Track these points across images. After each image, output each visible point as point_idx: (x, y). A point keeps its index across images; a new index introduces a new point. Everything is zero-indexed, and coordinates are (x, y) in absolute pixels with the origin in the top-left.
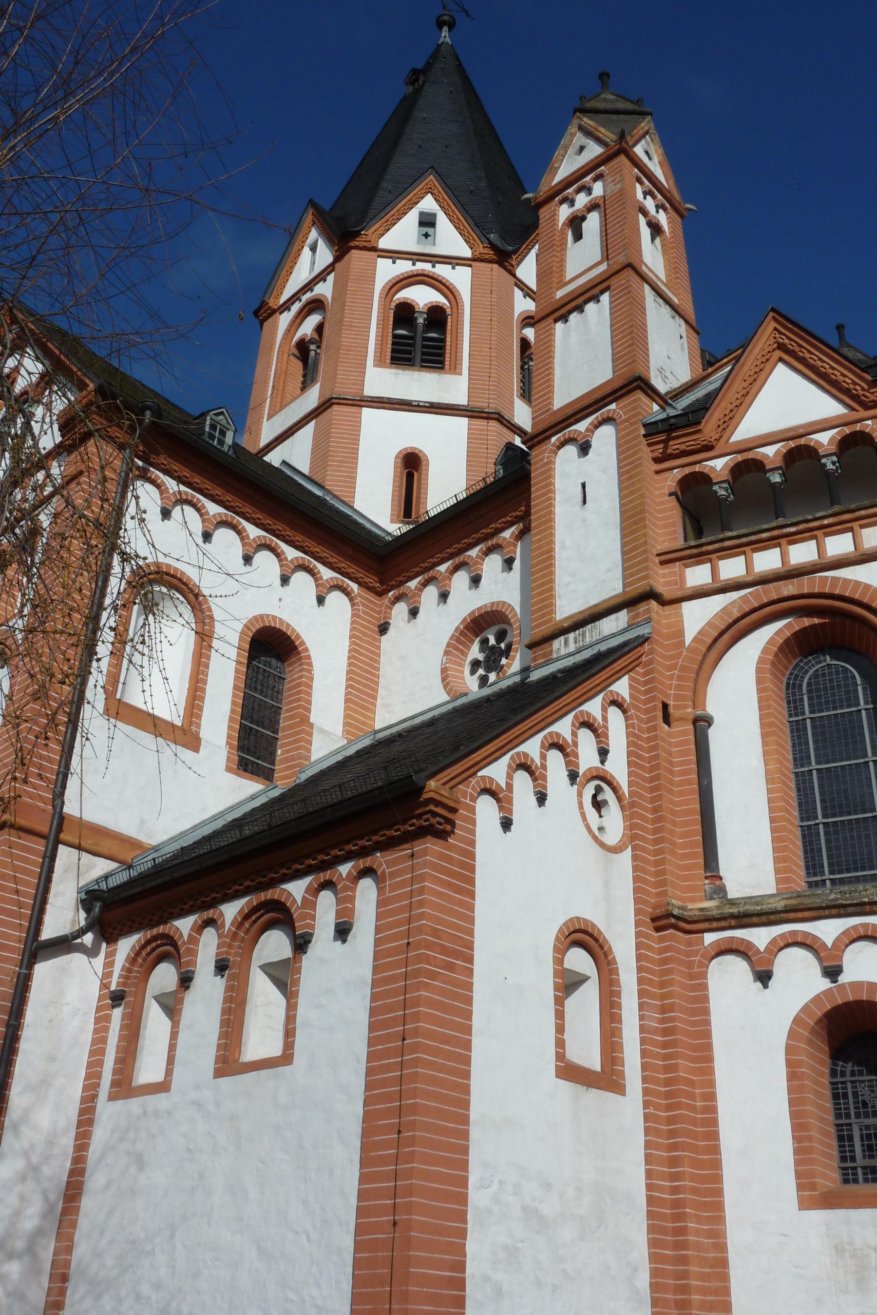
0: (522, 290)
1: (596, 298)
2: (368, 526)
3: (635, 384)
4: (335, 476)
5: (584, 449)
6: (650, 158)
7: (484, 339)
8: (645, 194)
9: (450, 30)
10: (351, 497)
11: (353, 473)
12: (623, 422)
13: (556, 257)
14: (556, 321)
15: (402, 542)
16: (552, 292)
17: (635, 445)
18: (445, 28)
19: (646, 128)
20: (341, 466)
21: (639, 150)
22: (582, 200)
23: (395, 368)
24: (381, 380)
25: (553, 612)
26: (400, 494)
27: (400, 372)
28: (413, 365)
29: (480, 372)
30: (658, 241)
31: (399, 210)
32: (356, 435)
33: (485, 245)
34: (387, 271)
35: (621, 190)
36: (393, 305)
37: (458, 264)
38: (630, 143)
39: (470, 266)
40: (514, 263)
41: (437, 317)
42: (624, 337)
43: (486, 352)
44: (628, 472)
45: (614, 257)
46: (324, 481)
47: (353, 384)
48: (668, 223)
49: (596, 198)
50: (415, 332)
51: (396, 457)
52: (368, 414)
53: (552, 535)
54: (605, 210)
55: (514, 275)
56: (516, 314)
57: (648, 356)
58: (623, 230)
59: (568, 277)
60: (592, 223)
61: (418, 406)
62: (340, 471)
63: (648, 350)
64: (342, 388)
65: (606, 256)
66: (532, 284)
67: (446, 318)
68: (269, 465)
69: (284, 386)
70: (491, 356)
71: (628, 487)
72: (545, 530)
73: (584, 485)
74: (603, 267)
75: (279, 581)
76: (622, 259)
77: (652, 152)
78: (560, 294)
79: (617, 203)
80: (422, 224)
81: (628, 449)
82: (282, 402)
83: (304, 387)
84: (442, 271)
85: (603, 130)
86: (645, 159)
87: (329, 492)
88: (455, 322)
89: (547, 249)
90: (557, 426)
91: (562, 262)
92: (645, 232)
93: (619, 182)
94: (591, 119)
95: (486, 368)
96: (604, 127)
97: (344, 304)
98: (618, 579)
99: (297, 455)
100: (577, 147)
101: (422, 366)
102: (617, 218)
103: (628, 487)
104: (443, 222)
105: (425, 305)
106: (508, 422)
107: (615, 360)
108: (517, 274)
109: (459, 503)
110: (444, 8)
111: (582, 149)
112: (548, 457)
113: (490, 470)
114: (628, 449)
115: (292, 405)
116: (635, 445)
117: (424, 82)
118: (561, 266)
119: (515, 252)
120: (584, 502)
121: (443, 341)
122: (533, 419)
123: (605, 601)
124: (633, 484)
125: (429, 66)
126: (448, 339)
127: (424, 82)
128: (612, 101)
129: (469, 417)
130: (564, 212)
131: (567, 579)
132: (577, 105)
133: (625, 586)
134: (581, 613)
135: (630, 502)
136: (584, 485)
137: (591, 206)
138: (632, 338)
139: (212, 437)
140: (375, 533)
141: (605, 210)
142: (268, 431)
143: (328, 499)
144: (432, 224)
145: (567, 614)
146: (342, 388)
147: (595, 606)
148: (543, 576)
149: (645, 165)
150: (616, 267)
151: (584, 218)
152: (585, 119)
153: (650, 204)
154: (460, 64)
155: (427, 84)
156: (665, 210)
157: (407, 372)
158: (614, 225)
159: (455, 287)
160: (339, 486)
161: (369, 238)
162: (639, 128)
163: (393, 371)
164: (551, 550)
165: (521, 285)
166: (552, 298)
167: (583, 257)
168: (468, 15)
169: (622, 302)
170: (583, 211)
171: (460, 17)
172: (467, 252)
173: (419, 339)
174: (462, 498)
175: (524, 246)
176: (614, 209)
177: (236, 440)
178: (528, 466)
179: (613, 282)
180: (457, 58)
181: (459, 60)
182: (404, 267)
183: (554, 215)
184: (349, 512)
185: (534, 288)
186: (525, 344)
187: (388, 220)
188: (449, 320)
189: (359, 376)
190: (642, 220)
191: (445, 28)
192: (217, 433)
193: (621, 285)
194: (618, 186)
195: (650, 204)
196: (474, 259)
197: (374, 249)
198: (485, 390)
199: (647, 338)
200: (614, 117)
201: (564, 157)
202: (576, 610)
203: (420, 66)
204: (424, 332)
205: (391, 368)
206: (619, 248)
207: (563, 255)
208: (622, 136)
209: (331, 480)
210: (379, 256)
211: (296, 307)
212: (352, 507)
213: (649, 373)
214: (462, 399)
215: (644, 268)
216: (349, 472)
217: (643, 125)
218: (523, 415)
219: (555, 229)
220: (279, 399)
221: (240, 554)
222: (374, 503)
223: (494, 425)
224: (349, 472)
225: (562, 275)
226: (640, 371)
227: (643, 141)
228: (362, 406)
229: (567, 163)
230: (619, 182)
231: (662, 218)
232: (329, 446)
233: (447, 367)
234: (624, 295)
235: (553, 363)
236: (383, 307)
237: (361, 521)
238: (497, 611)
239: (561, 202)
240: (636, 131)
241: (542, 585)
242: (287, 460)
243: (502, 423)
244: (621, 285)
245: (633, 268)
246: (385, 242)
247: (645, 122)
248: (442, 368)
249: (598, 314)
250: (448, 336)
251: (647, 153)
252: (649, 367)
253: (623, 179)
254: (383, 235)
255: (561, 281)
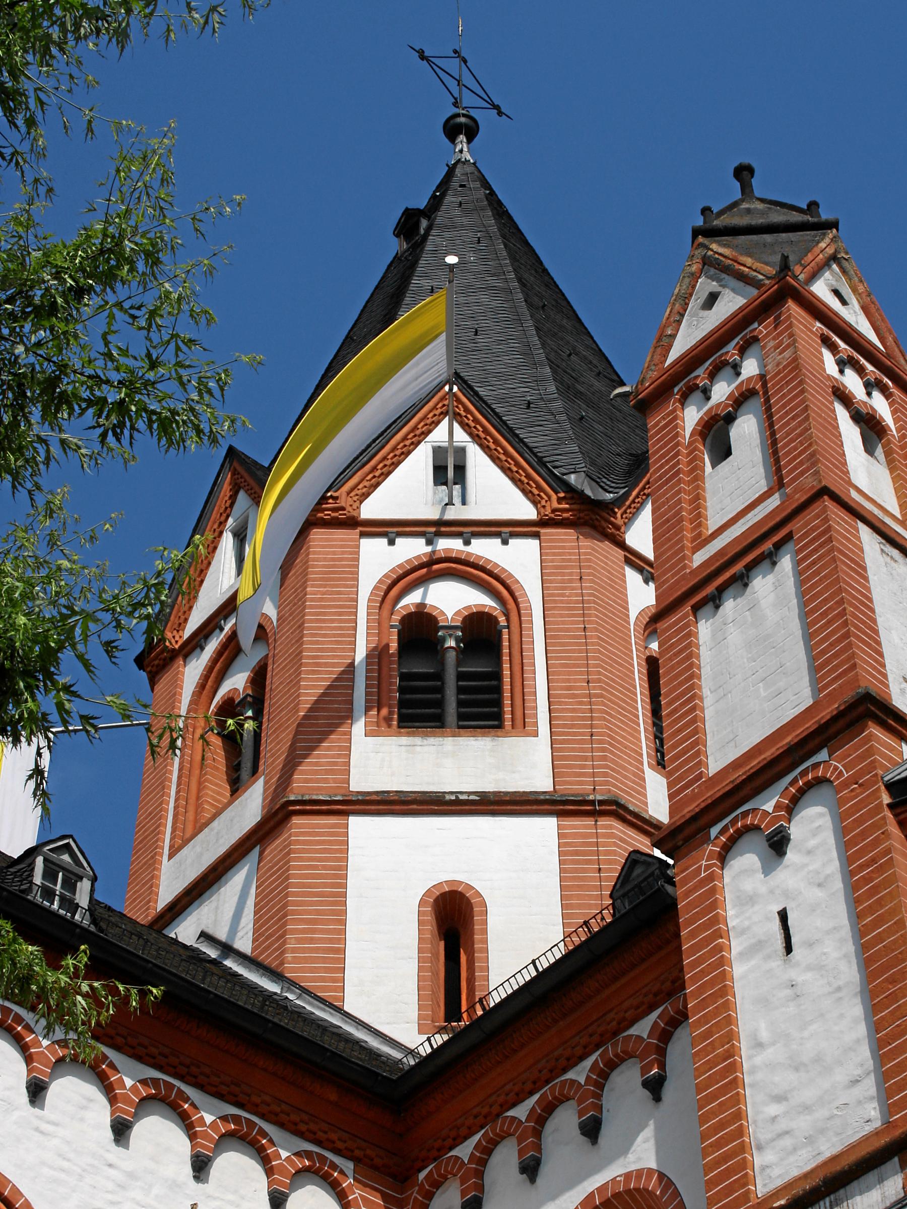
0: (640, 570)
1: (771, 558)
2: (374, 1043)
3: (861, 709)
4: (304, 950)
5: (778, 844)
6: (844, 302)
7: (575, 666)
8: (842, 364)
9: (469, 141)
10: (335, 989)
11: (339, 941)
12: (845, 785)
13: (685, 491)
14: (696, 609)
15: (435, 1070)
16: (684, 558)
17: (875, 827)
18: (462, 138)
19: (830, 251)
20: (314, 931)
21: (821, 289)
22: (721, 391)
23: (409, 735)
24: (378, 757)
25: (745, 1181)
26: (435, 974)
27: (417, 740)
28: (442, 726)
29: (572, 726)
30: (879, 451)
31: (394, 449)
32: (340, 868)
33: (562, 495)
34: (378, 559)
35: (795, 359)
36: (396, 618)
37: (514, 535)
38: (802, 277)
39: (536, 535)
40: (619, 521)
41: (483, 636)
42: (829, 623)
43: (582, 688)
44: (867, 880)
45: (794, 480)
46: (282, 963)
47: (327, 772)
48: (894, 413)
49: (750, 379)
50: (442, 663)
51: (422, 903)
52: (360, 827)
53: (730, 1021)
54: (767, 400)
55: (621, 544)
56: (633, 615)
57: (881, 655)
58: (806, 430)
59: (713, 523)
60: (746, 430)
61: (458, 802)
62: (312, 940)
63: (879, 643)
64: (307, 781)
65: (778, 482)
66: (647, 549)
67: (500, 633)
68: (175, 941)
69: (199, 790)
70: (590, 696)
71: (871, 910)
72: (716, 1012)
73: (783, 916)
74: (774, 502)
75: (188, 1170)
76: (809, 483)
77: (846, 292)
78: (699, 559)
79: (787, 383)
80: (440, 474)
81: (863, 835)
82: (196, 821)
83: (236, 786)
84: (485, 549)
85: (749, 261)
86: (834, 303)
87: (292, 984)
88: (516, 639)
89: (667, 482)
90: (729, 811)
91: (697, 501)
92: (850, 434)
93: (788, 346)
94: (725, 246)
95: (583, 719)
96: (750, 255)
97: (301, 627)
98: (872, 1098)
99: (225, 918)
100: (704, 295)
101: (459, 727)
102: (792, 410)
103: (871, 910)
104: (478, 462)
105: (458, 613)
106: (637, 816)
107: (817, 667)
108: (628, 542)
109: (541, 976)
110: (456, 104)
111: (712, 299)
112: (708, 867)
113: (598, 906)
114: (863, 835)
115: (215, 824)
116: (875, 827)
117: (429, 228)
118: (698, 507)
119: (619, 502)
120: (789, 949)
121: (497, 676)
122: (671, 797)
123: (852, 1148)
124: (880, 903)
125: (436, 202)
126: (507, 672)
127: (429, 228)
128: (762, 213)
129: (560, 814)
130: (691, 416)
131: (773, 1109)
132: (700, 222)
133: (888, 1109)
134: (806, 1176)
135: (879, 938)
136: (783, 916)
137: (742, 394)
138: (846, 623)
139: (49, 894)
140: (388, 1057)
141: (767, 400)
142: (172, 878)
143: (291, 997)
144: (461, 469)
145: (779, 1183)
146: (307, 781)
147: (834, 1159)
148: (722, 1107)
149: (836, 314)
150: (801, 498)
151: (730, 419)
152: (714, 246)
153: (853, 382)
154: (492, 193)
155: (433, 232)
156: (884, 390)
157: (431, 740)
158: (787, 423)
159: (511, 576)
160: (312, 970)
161: (342, 503)
162: (816, 250)
163: (404, 740)
164: (732, 1053)
165: (634, 559)
166: (685, 567)
167: (735, 489)
168: (500, 113)
169: (819, 559)
170: (727, 406)
171: (485, 118)
172: (527, 511)
173: (448, 677)
174: (546, 965)
175: (634, 493)
176: (784, 396)
177: (97, 896)
178: (669, 888)
179: (795, 525)
180: (486, 184)
181: (490, 188)
182: (412, 549)
183: (674, 422)
184: (335, 1020)
185: (650, 554)
186: (652, 665)
187: (374, 469)
188: (505, 636)
189: (339, 756)
190: (842, 414)
191: (462, 138)
192: (58, 887)
193: (813, 529)
194: (787, 354)
195: (853, 382)
196: (543, 522)
197: (352, 523)
198: (585, 759)
199: (874, 621)
200: (768, 238)
201: (682, 316)
202: (795, 1173)
203: (422, 204)
204: (459, 663)
205: (399, 735)
206: (801, 463)
207: (698, 487)
208: (785, 266)
209: (296, 960)
210: (363, 535)
211: (212, 646)
212: (339, 1010)
213: (887, 686)
214: (540, 781)
215: (854, 494)
216: (331, 941)
217: (823, 245)
218: (657, 802)
219: (678, 444)
220: (191, 815)
221: (107, 1120)
222: (384, 996)
223: (612, 826)
224: (331, 941)
225: (700, 525)
226: (868, 682)
227: (827, 274)
228: (347, 813)
229: (689, 325)
230: (788, 346)
231: (880, 405)
232: (287, 895)
233: (508, 723)
234: (821, 546)
235: (700, 688)
236: (377, 625)
237: (360, 1034)
238: (637, 1190)
239: (684, 399)
240: (810, 256)
241: (722, 1125)
242: (210, 931)
243: (624, 820)
244: (813, 529)
245: (831, 495)
246: (372, 508)
247: (827, 240)
248: (500, 726)
249: (774, 591)
250: (506, 666)
251: (837, 293)
252: (885, 676)
253: (795, 341)
254: (366, 495)
255: (700, 534)
